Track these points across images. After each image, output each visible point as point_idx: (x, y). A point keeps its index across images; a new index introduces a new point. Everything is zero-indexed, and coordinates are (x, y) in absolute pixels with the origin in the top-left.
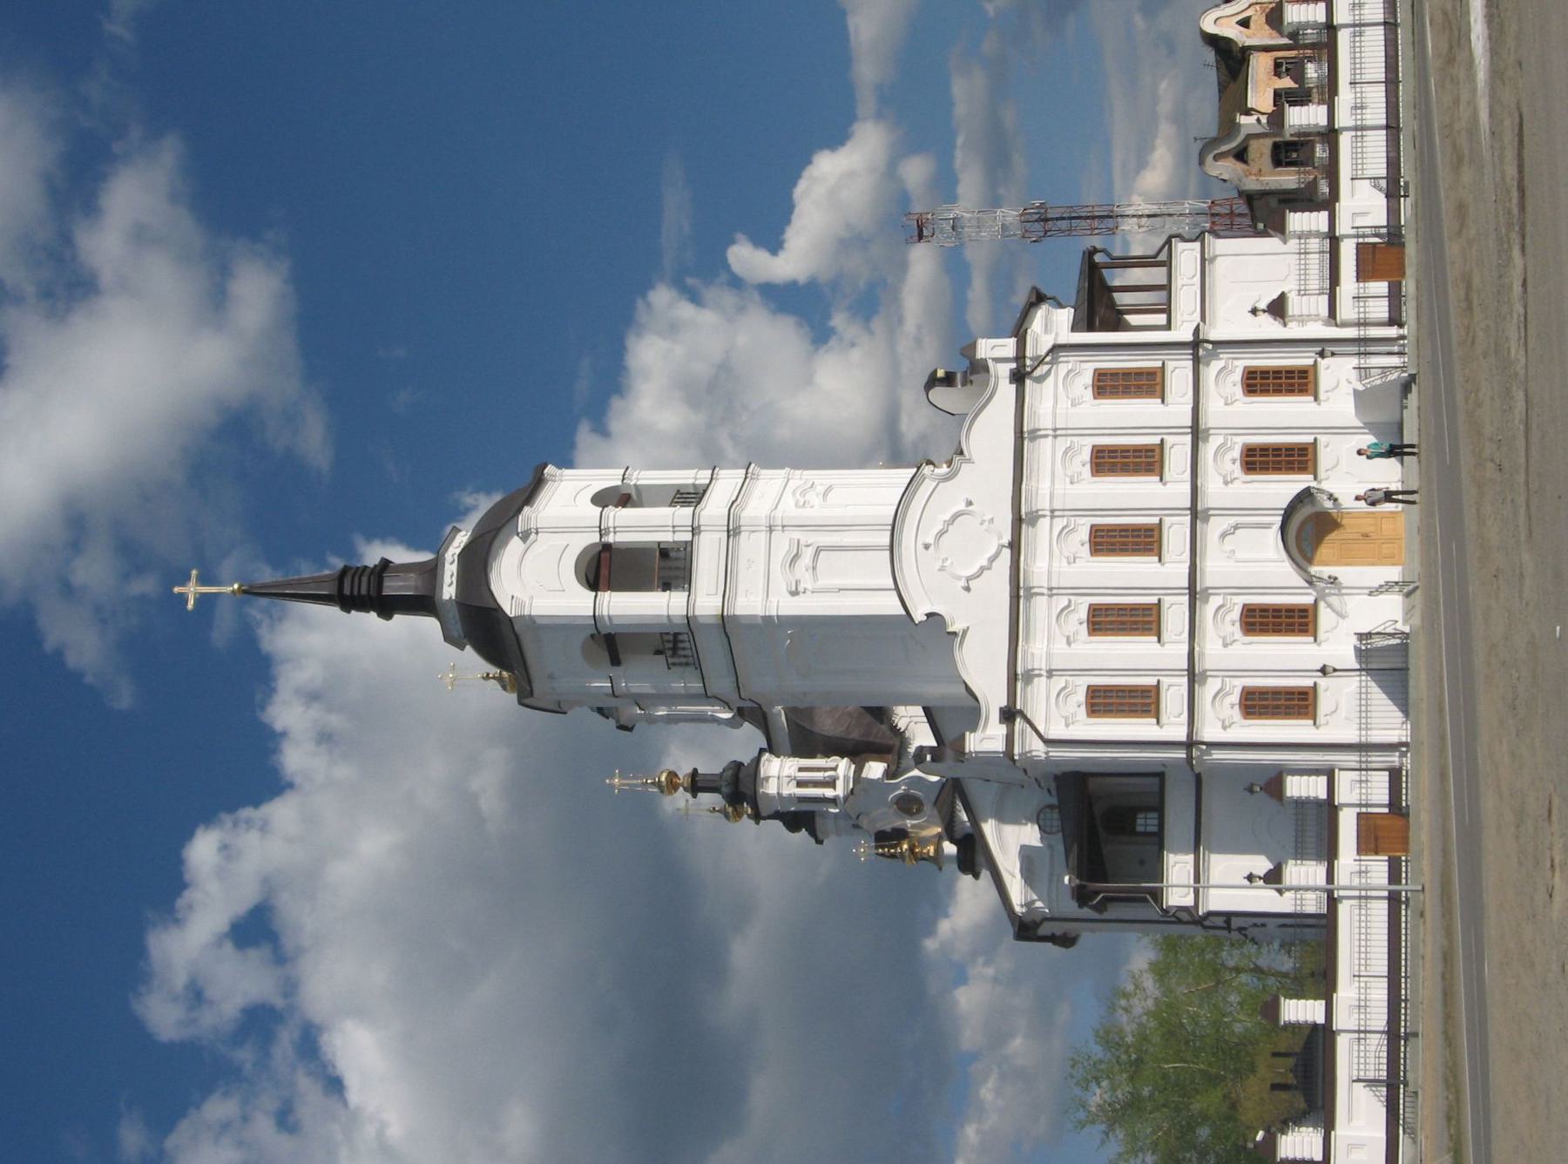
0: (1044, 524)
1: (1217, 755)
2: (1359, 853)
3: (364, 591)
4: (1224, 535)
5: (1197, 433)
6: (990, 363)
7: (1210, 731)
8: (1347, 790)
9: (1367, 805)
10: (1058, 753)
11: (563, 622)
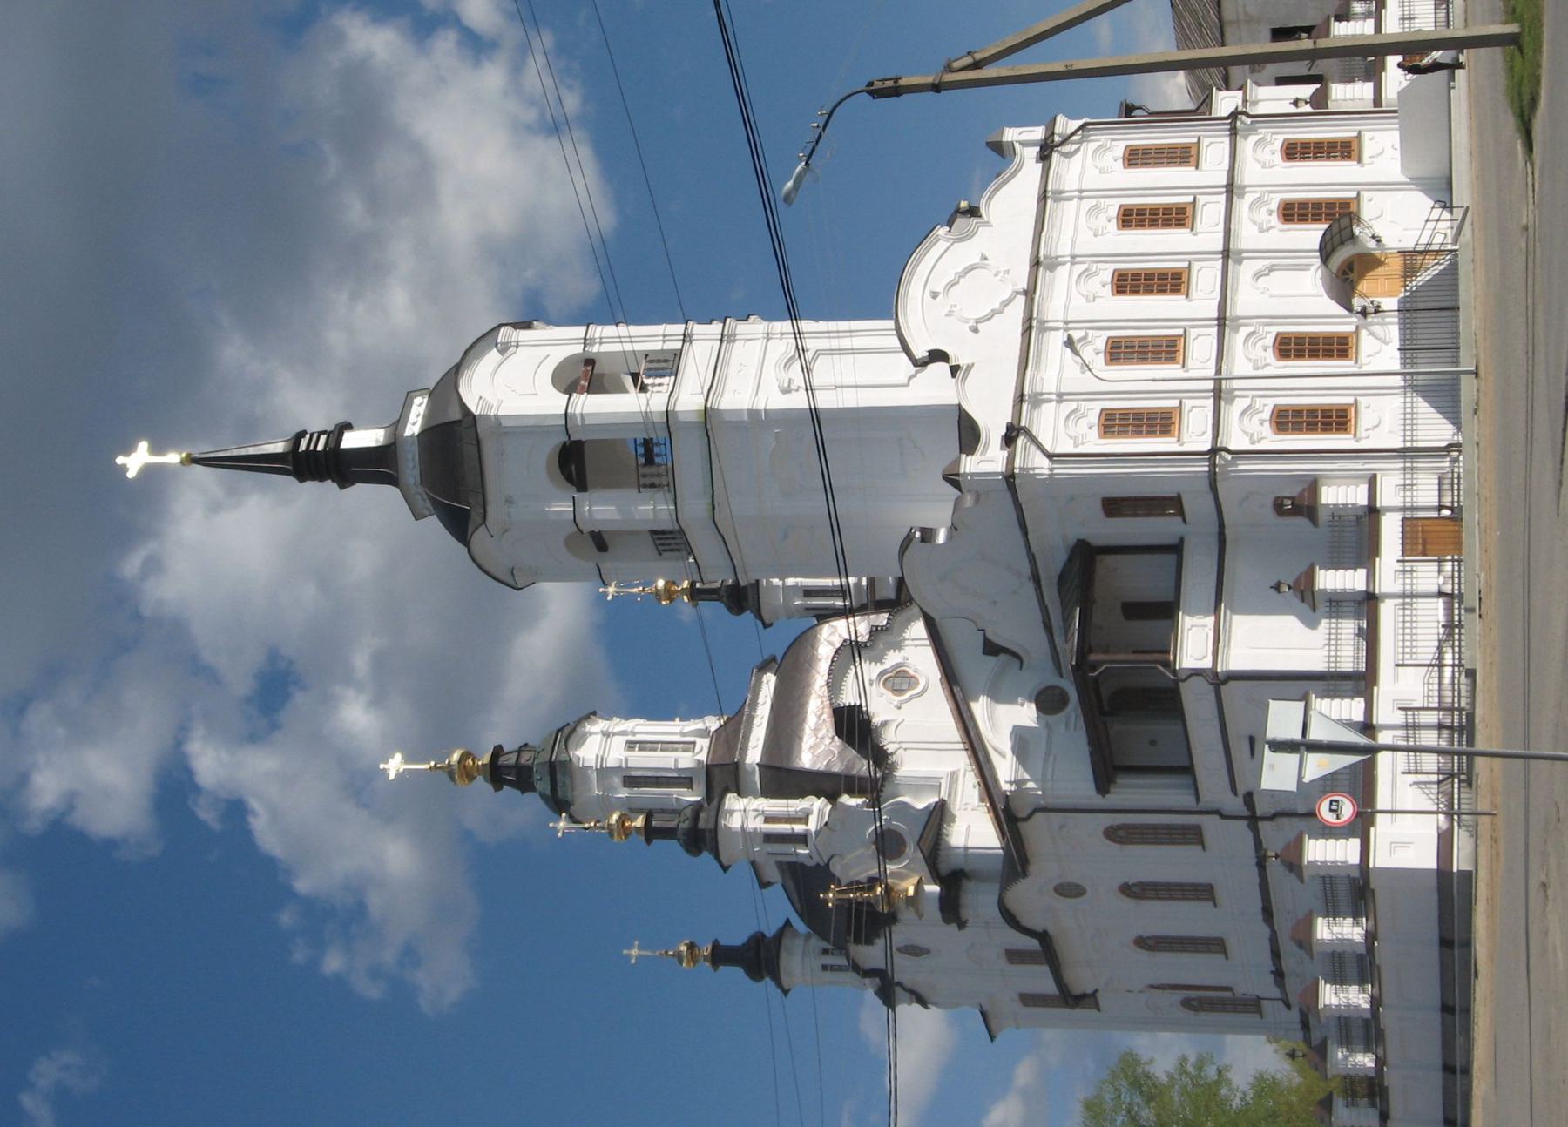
0: (1062, 271)
1: (1244, 466)
2: (1404, 553)
3: (320, 448)
4: (1258, 276)
5: (1231, 189)
6: (1017, 146)
7: (1236, 439)
8: (1388, 495)
9: (1413, 509)
10: (1063, 470)
11: (531, 423)
